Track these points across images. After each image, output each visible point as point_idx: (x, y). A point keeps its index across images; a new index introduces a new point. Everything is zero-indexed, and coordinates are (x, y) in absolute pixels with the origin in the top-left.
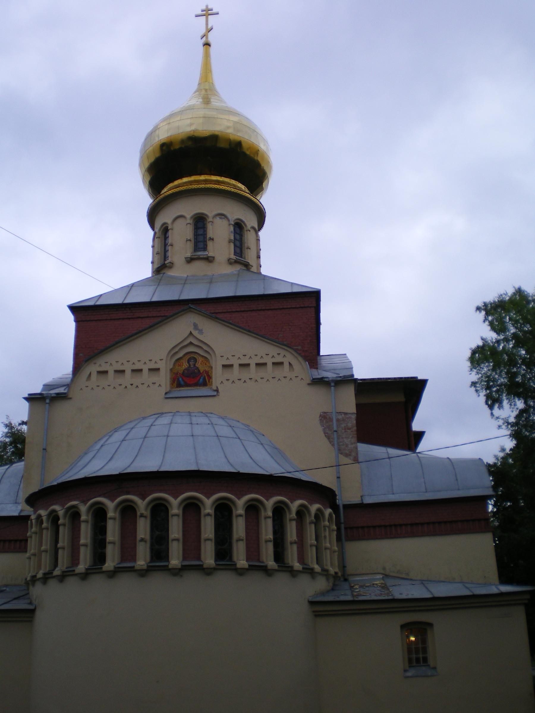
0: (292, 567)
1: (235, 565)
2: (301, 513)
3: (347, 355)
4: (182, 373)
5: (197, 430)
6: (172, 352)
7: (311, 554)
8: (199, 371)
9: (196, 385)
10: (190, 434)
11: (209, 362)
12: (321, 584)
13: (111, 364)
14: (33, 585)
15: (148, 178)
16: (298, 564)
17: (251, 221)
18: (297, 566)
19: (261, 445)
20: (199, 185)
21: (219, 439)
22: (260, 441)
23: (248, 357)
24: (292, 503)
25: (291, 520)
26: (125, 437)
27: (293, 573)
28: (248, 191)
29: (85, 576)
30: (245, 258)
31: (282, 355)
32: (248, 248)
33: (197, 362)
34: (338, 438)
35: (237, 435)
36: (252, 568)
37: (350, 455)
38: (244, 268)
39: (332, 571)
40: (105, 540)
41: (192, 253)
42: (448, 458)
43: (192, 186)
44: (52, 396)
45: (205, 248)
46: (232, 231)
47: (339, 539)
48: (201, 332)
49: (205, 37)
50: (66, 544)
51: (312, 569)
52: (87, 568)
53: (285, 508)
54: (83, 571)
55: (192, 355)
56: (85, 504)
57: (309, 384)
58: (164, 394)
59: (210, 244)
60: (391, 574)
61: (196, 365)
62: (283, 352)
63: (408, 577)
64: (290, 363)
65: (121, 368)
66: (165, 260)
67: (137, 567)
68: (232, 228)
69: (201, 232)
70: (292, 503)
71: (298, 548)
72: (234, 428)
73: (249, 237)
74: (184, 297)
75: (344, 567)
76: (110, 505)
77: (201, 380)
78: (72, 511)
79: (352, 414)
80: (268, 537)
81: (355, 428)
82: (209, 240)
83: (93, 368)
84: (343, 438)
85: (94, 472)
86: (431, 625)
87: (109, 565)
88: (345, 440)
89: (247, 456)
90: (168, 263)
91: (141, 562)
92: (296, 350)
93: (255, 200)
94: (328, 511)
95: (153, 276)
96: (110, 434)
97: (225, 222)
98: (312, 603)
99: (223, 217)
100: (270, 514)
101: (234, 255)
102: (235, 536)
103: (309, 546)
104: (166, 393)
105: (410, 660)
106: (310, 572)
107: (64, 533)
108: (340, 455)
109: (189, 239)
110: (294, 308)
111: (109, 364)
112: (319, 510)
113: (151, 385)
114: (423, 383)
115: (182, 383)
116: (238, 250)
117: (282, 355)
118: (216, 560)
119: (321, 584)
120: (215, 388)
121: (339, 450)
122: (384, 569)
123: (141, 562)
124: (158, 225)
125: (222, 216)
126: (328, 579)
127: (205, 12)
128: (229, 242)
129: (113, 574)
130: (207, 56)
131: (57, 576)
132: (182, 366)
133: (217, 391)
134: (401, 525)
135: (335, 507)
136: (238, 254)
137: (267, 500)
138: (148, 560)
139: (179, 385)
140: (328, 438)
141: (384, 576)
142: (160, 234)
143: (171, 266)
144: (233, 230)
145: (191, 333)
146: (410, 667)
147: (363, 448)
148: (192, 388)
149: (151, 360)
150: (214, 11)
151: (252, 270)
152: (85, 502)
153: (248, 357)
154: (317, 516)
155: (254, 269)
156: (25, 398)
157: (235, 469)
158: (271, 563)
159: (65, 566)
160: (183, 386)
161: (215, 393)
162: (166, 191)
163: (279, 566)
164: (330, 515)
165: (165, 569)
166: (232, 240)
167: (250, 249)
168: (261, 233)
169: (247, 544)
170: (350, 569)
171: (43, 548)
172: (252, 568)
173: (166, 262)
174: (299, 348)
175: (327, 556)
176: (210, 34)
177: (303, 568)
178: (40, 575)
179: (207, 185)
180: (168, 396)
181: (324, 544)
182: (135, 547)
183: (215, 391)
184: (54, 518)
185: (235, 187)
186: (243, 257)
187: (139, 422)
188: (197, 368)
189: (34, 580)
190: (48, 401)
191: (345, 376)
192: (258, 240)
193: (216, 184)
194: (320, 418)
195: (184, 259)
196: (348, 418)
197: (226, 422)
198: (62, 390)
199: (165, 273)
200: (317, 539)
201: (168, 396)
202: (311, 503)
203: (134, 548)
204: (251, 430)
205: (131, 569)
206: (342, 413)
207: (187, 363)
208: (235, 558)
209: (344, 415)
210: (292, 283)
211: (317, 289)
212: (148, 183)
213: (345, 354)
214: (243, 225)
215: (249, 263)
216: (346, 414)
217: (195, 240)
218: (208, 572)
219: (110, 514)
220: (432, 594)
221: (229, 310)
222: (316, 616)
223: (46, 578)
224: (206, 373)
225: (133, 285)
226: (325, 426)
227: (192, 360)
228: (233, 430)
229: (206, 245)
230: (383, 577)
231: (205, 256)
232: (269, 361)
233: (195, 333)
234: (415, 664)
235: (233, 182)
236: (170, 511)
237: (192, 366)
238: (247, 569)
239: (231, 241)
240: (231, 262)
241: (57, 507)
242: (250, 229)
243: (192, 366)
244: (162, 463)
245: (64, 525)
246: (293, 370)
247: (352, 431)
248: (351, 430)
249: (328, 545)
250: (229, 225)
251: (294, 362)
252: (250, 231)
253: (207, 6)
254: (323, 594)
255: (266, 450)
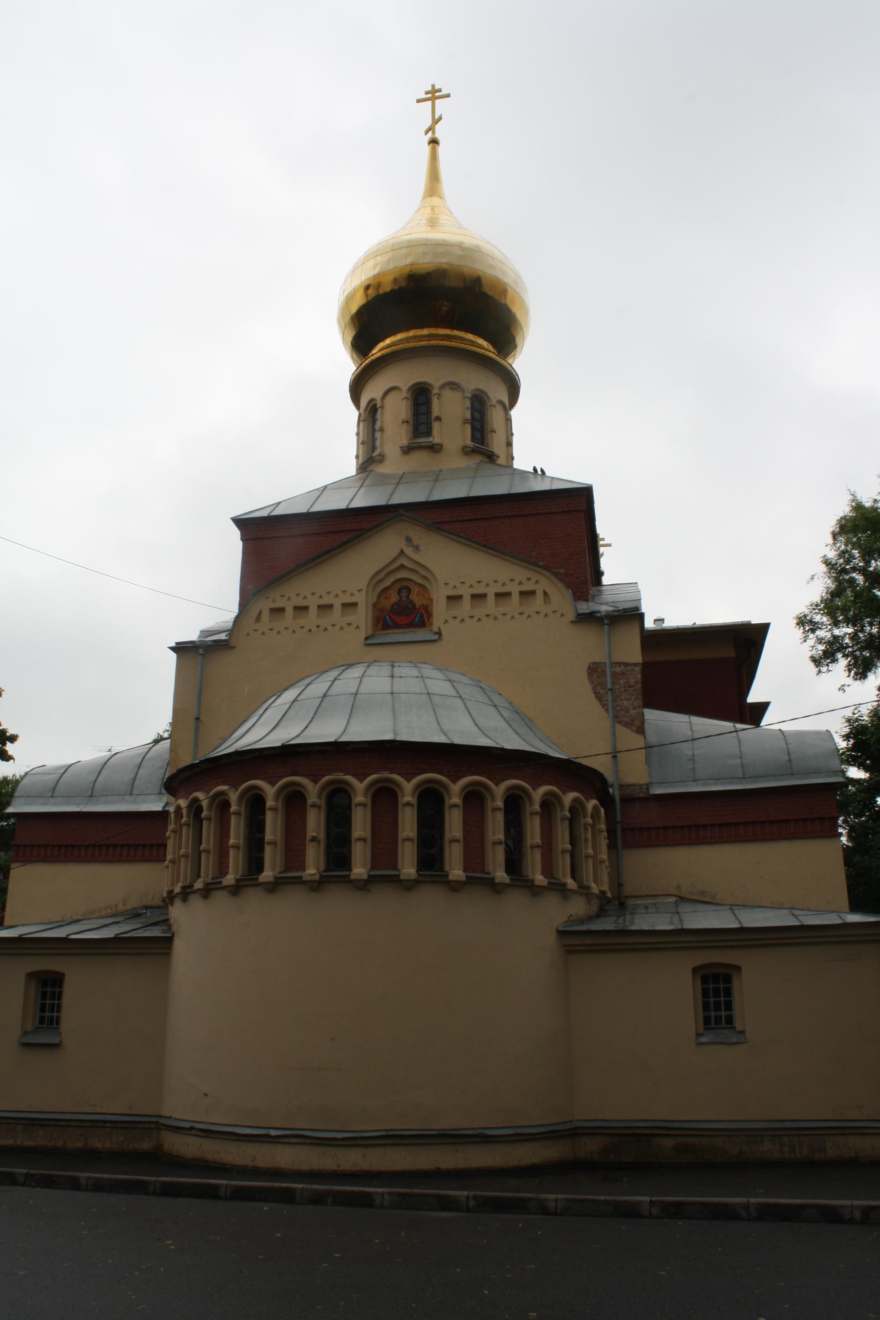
0: (533, 881)
1: (447, 875)
2: (548, 805)
3: (638, 584)
4: (389, 610)
5: (400, 685)
6: (376, 580)
7: (563, 864)
8: (414, 605)
9: (411, 625)
10: (389, 691)
11: (428, 593)
12: (578, 907)
13: (289, 598)
14: (172, 903)
15: (350, 335)
16: (541, 877)
17: (497, 392)
18: (540, 879)
19: (493, 707)
20: (420, 343)
21: (430, 699)
22: (492, 701)
23: (484, 584)
24: (534, 789)
25: (532, 814)
26: (296, 698)
27: (534, 890)
28: (493, 350)
29: (236, 890)
30: (487, 446)
31: (533, 580)
32: (493, 431)
33: (412, 593)
34: (614, 700)
35: (458, 692)
36: (470, 881)
37: (632, 725)
38: (486, 460)
39: (595, 889)
40: (263, 839)
41: (410, 440)
42: (780, 730)
43: (410, 344)
44: (208, 644)
45: (429, 433)
46: (469, 407)
47: (612, 846)
48: (417, 548)
49: (431, 132)
50: (211, 845)
51: (564, 885)
52: (237, 878)
53: (523, 795)
54: (232, 882)
55: (405, 583)
56: (237, 789)
57: (572, 622)
58: (363, 638)
59: (436, 426)
60: (689, 896)
61: (410, 598)
62: (535, 576)
63: (714, 901)
64: (545, 593)
65: (304, 603)
66: (373, 452)
67: (305, 878)
68: (468, 403)
69: (423, 409)
70: (534, 789)
71: (543, 854)
72: (455, 684)
73: (495, 416)
74: (395, 501)
75: (620, 885)
76: (270, 791)
77: (417, 618)
78: (219, 799)
79: (636, 665)
80: (496, 837)
81: (640, 685)
82: (434, 421)
83: (264, 605)
84: (621, 700)
85: (250, 745)
86: (738, 968)
87: (267, 875)
88: (625, 703)
89: (471, 721)
90: (376, 456)
91: (311, 871)
92: (556, 575)
93: (506, 364)
94: (592, 804)
95: (356, 475)
96: (279, 694)
97: (457, 395)
98: (561, 933)
99: (455, 387)
100: (500, 804)
101: (472, 441)
102: (447, 836)
103: (560, 853)
104: (367, 638)
105: (707, 1021)
106: (559, 888)
107: (209, 830)
108: (618, 726)
109: (405, 420)
110: (554, 513)
111: (286, 598)
112: (575, 800)
113: (345, 626)
114: (764, 628)
115: (390, 623)
116: (478, 435)
117: (533, 580)
118: (418, 870)
119: (578, 907)
120: (436, 629)
121: (616, 717)
122: (679, 887)
123: (311, 871)
124: (364, 403)
125: (453, 386)
126: (589, 901)
127: (430, 95)
128: (464, 423)
129: (274, 887)
130: (434, 157)
131: (199, 890)
132: (390, 599)
133: (439, 633)
134: (705, 826)
135: (606, 800)
136: (478, 439)
137: (497, 784)
138: (322, 867)
139: (386, 627)
140: (599, 698)
141: (678, 898)
142: (367, 415)
143: (381, 459)
144: (470, 406)
145: (402, 552)
146: (705, 1029)
147: (652, 716)
148: (405, 630)
149: (346, 591)
150: (444, 92)
151: (499, 461)
152: (235, 787)
153: (484, 584)
154: (572, 810)
155: (502, 460)
156: (172, 648)
157: (449, 739)
158: (501, 875)
159: (210, 876)
160: (390, 628)
161: (437, 637)
162: (377, 352)
163: (511, 879)
164: (595, 808)
165: (346, 881)
166: (467, 419)
167: (495, 432)
168: (514, 413)
169: (464, 846)
170: (628, 890)
171: (182, 851)
172: (470, 881)
173: (374, 455)
174: (562, 571)
175: (588, 868)
176: (438, 127)
177: (549, 883)
178: (177, 890)
179: (430, 342)
180: (369, 642)
181: (583, 850)
182: (304, 850)
183: (436, 633)
184: (196, 808)
185: (473, 343)
186: (485, 444)
187: (318, 677)
188: (412, 602)
189: (171, 897)
190: (201, 651)
191: (626, 609)
192: (508, 420)
193: (444, 340)
194: (589, 671)
195: (399, 450)
196: (629, 671)
197: (444, 674)
198: (223, 636)
199: (372, 470)
200: (573, 842)
201: (369, 642)
202: (588, 798)
203: (303, 852)
204: (481, 687)
205: (299, 881)
206: (621, 663)
207: (396, 595)
208: (447, 868)
209: (624, 666)
210: (552, 478)
211: (587, 484)
212: (350, 345)
213: (636, 583)
214: (485, 397)
215: (493, 452)
216: (626, 665)
217: (415, 422)
218: (409, 886)
219: (270, 803)
220: (740, 923)
221: (459, 519)
222: (569, 952)
223: (186, 893)
224: (424, 609)
225: (325, 488)
226: (595, 683)
227: (404, 591)
228: (454, 686)
229: (431, 428)
230: (677, 900)
231: (428, 444)
232: (515, 589)
233: (408, 551)
234: (713, 1026)
235: (470, 336)
236: (353, 798)
237: (404, 599)
238: (463, 882)
239: (466, 421)
240: (467, 452)
241: (200, 795)
242: (495, 404)
243: (404, 599)
244: (344, 731)
245: (209, 819)
246: (550, 602)
247: (635, 690)
248: (634, 688)
249: (590, 851)
250: (464, 398)
251: (551, 590)
252: (495, 406)
253: (433, 86)
254: (582, 921)
255: (501, 714)
